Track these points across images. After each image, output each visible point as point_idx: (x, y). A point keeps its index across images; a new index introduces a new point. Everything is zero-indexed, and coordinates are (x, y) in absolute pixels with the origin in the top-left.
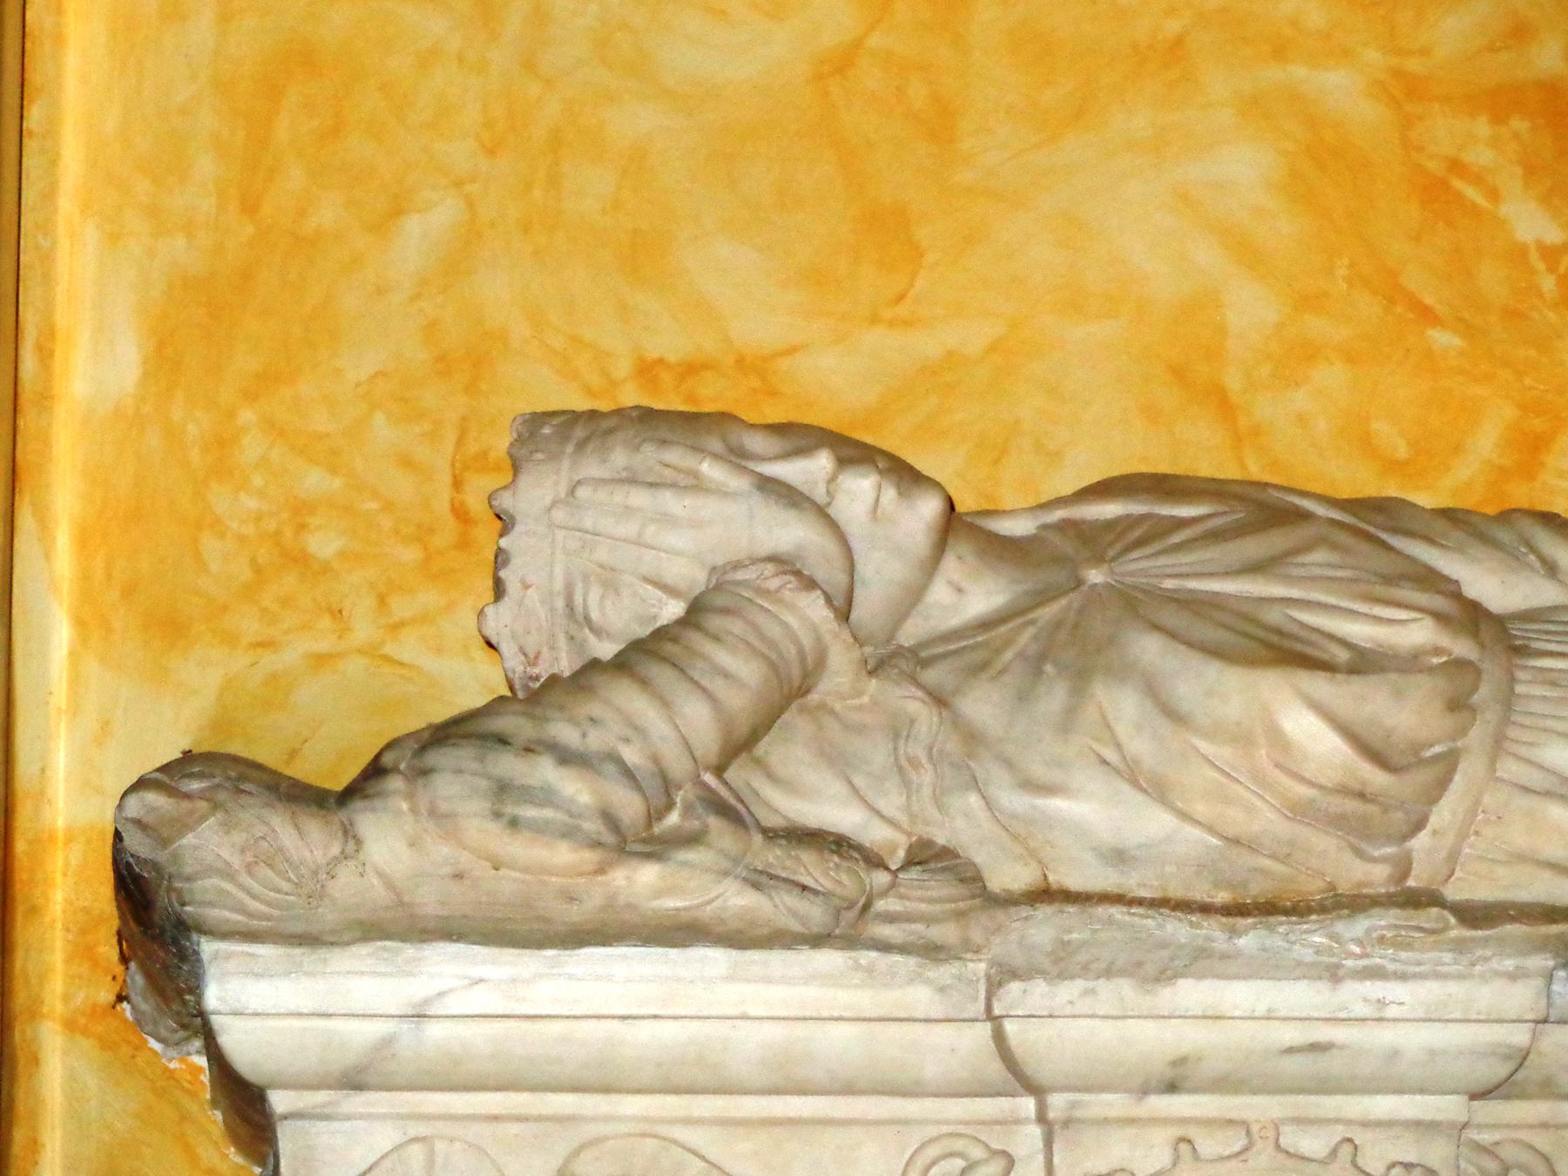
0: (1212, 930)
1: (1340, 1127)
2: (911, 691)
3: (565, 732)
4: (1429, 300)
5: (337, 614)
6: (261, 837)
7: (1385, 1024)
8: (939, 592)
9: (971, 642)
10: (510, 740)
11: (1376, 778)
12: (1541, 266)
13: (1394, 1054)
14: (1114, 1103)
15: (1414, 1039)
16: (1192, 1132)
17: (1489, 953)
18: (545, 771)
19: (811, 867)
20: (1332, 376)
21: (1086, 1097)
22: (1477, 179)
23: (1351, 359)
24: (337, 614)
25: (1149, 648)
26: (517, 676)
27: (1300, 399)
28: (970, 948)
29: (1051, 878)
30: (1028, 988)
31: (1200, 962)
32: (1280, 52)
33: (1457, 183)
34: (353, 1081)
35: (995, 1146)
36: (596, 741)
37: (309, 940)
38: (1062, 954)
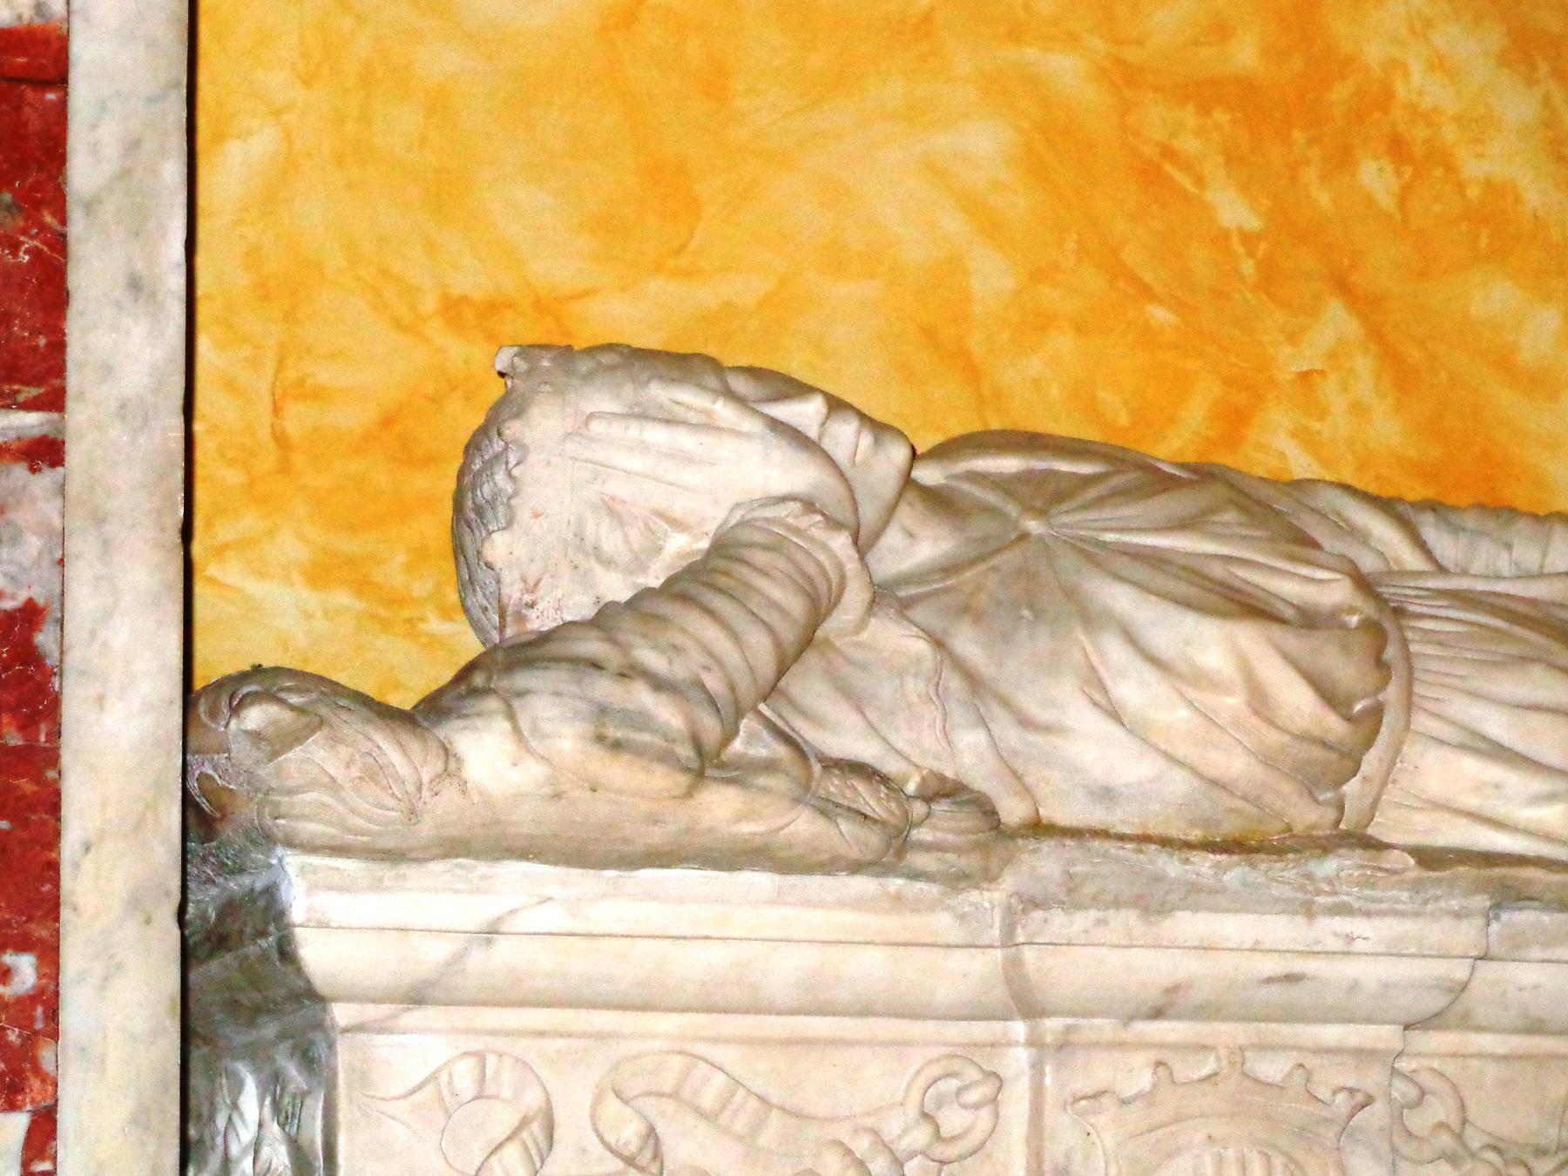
0: (1204, 864)
1: (1295, 1054)
2: (912, 631)
4: (1147, 277)
6: (367, 753)
7: (1351, 957)
9: (941, 585)
10: (604, 665)
12: (1239, 249)
13: (1355, 986)
14: (1104, 1027)
15: (1370, 972)
16: (1167, 1056)
17: (1439, 893)
18: (642, 697)
19: (866, 797)
20: (1063, 343)
21: (1083, 1022)
22: (1187, 166)
23: (1080, 329)
25: (1120, 598)
26: (512, 602)
27: (1035, 365)
28: (988, 877)
29: (1042, 812)
30: (1049, 917)
31: (1196, 896)
32: (1015, 34)
33: (1168, 168)
34: (416, 997)
35: (988, 1068)
36: (679, 670)
37: (394, 856)
38: (1072, 885)
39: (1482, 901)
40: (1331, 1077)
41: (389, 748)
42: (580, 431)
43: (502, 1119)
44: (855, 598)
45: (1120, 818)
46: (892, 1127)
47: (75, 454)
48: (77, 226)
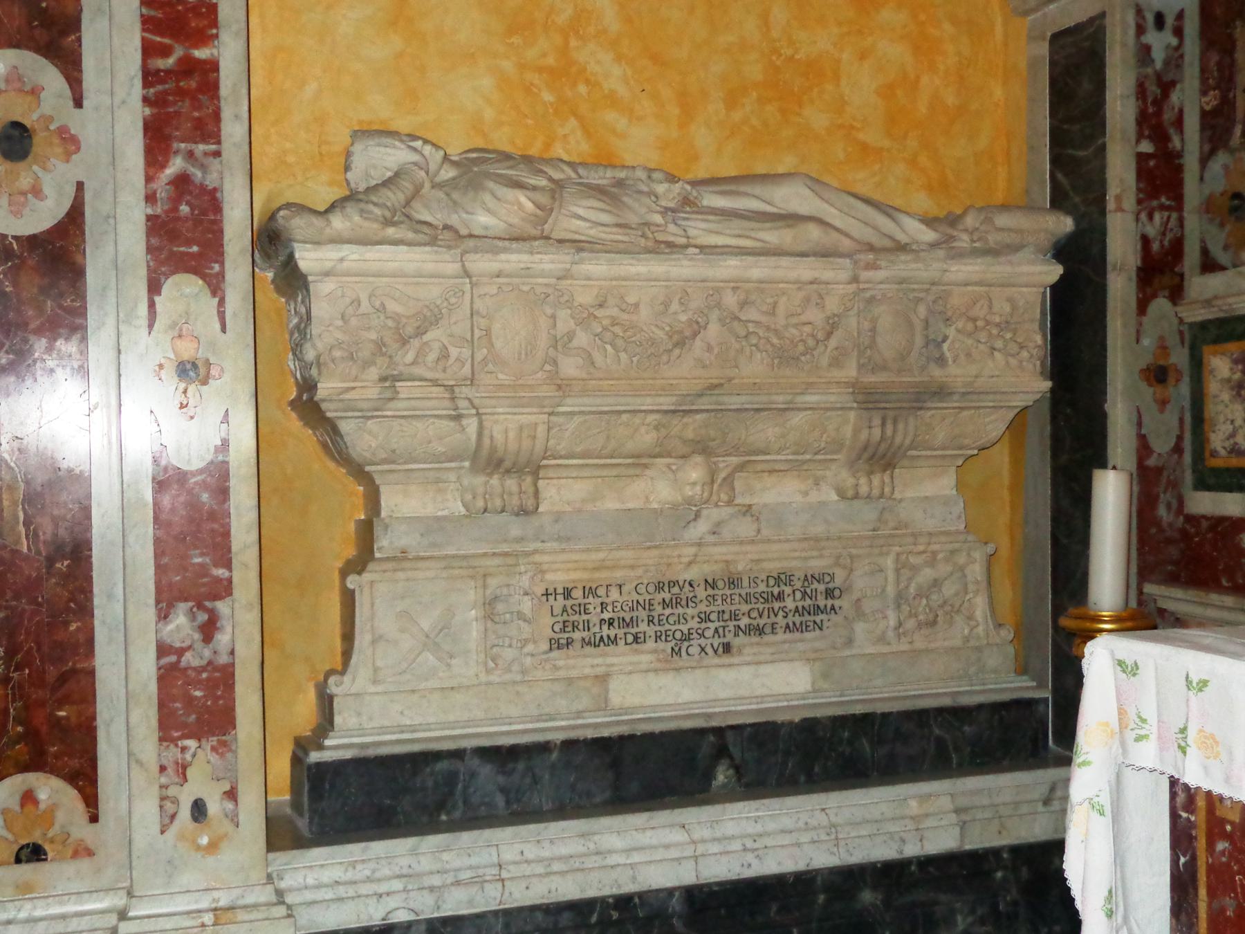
0: (507, 243)
3: (374, 199)
5: (294, 176)
8: (442, 172)
11: (539, 212)
15: (547, 267)
18: (371, 207)
19: (426, 229)
24: (294, 176)
25: (491, 185)
28: (456, 247)
31: (505, 250)
34: (327, 274)
36: (381, 201)
39: (573, 251)
40: (539, 290)
41: (318, 222)
42: (366, 149)
43: (348, 300)
44: (427, 185)
45: (489, 233)
46: (438, 302)
47: (224, 154)
48: (223, 103)
